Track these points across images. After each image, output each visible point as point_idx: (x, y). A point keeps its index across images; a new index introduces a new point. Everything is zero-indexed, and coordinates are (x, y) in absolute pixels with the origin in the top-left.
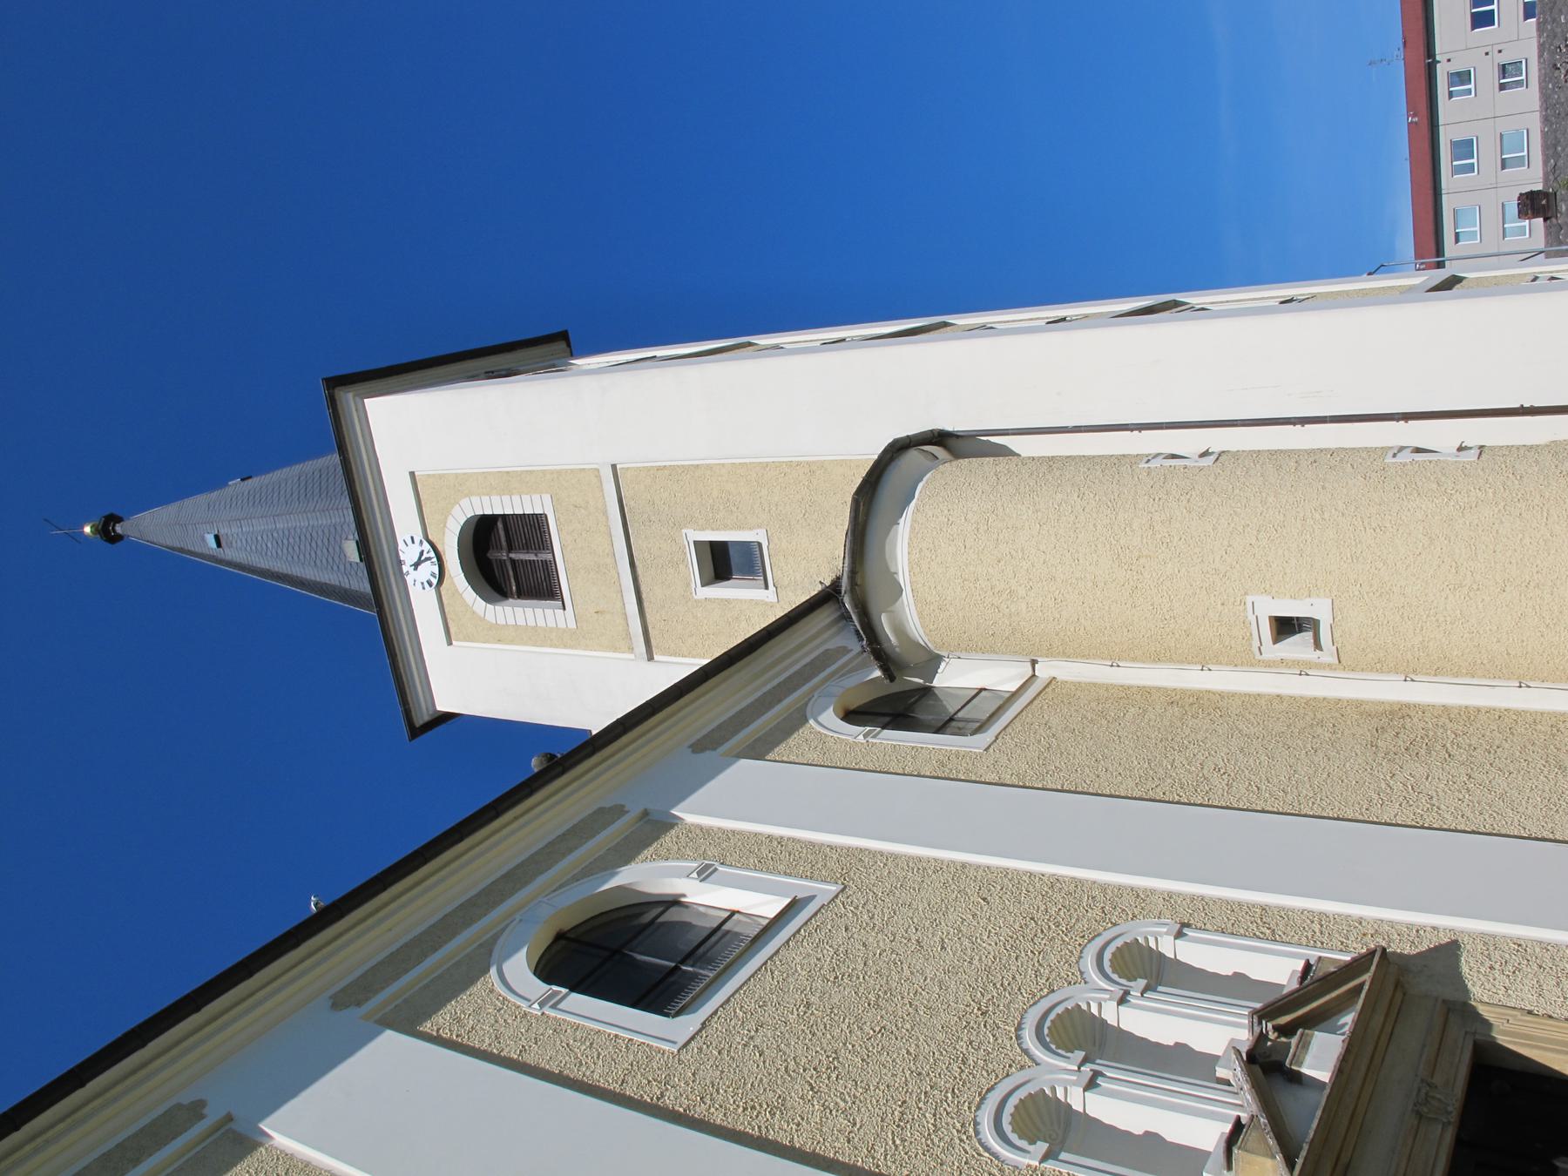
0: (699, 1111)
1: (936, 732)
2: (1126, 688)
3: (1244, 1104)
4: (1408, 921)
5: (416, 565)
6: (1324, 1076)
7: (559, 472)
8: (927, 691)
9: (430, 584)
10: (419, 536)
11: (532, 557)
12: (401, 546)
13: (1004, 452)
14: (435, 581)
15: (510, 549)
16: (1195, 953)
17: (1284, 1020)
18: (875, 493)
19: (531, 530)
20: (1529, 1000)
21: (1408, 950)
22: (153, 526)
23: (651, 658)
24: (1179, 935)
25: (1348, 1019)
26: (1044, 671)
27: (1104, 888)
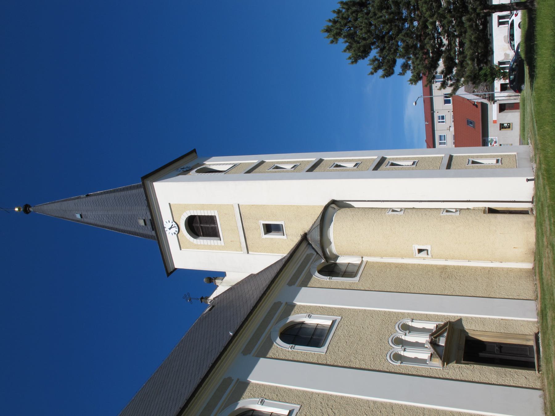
0: (336, 364)
2: (385, 263)
3: (432, 350)
4: (453, 315)
5: (170, 229)
6: (443, 344)
7: (220, 205)
8: (336, 264)
9: (175, 233)
10: (171, 220)
11: (208, 226)
12: (165, 223)
13: (350, 206)
14: (177, 233)
15: (201, 223)
16: (416, 324)
17: (435, 336)
18: (324, 220)
19: (211, 220)
20: (474, 328)
21: (453, 321)
22: (51, 208)
23: (248, 253)
24: (412, 321)
25: (445, 334)
26: (365, 259)
27: (395, 313)
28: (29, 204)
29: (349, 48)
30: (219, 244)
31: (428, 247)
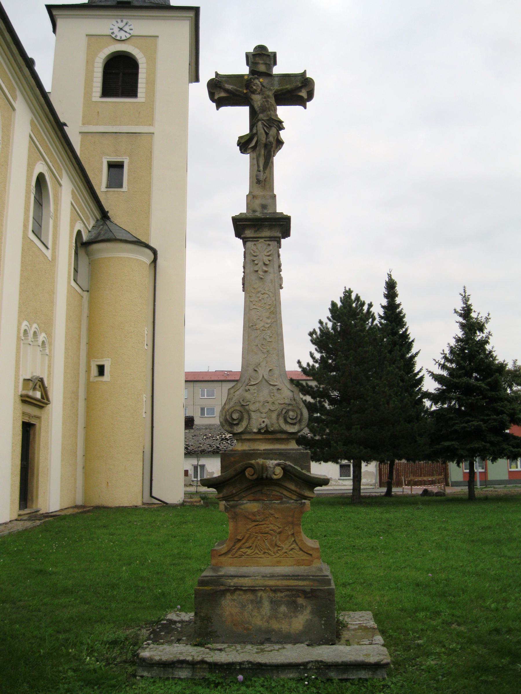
1: (74, 269)
9: (113, 33)
14: (114, 36)
28: (297, 361)
29: (458, 340)
30: (94, 94)
31: (107, 377)
